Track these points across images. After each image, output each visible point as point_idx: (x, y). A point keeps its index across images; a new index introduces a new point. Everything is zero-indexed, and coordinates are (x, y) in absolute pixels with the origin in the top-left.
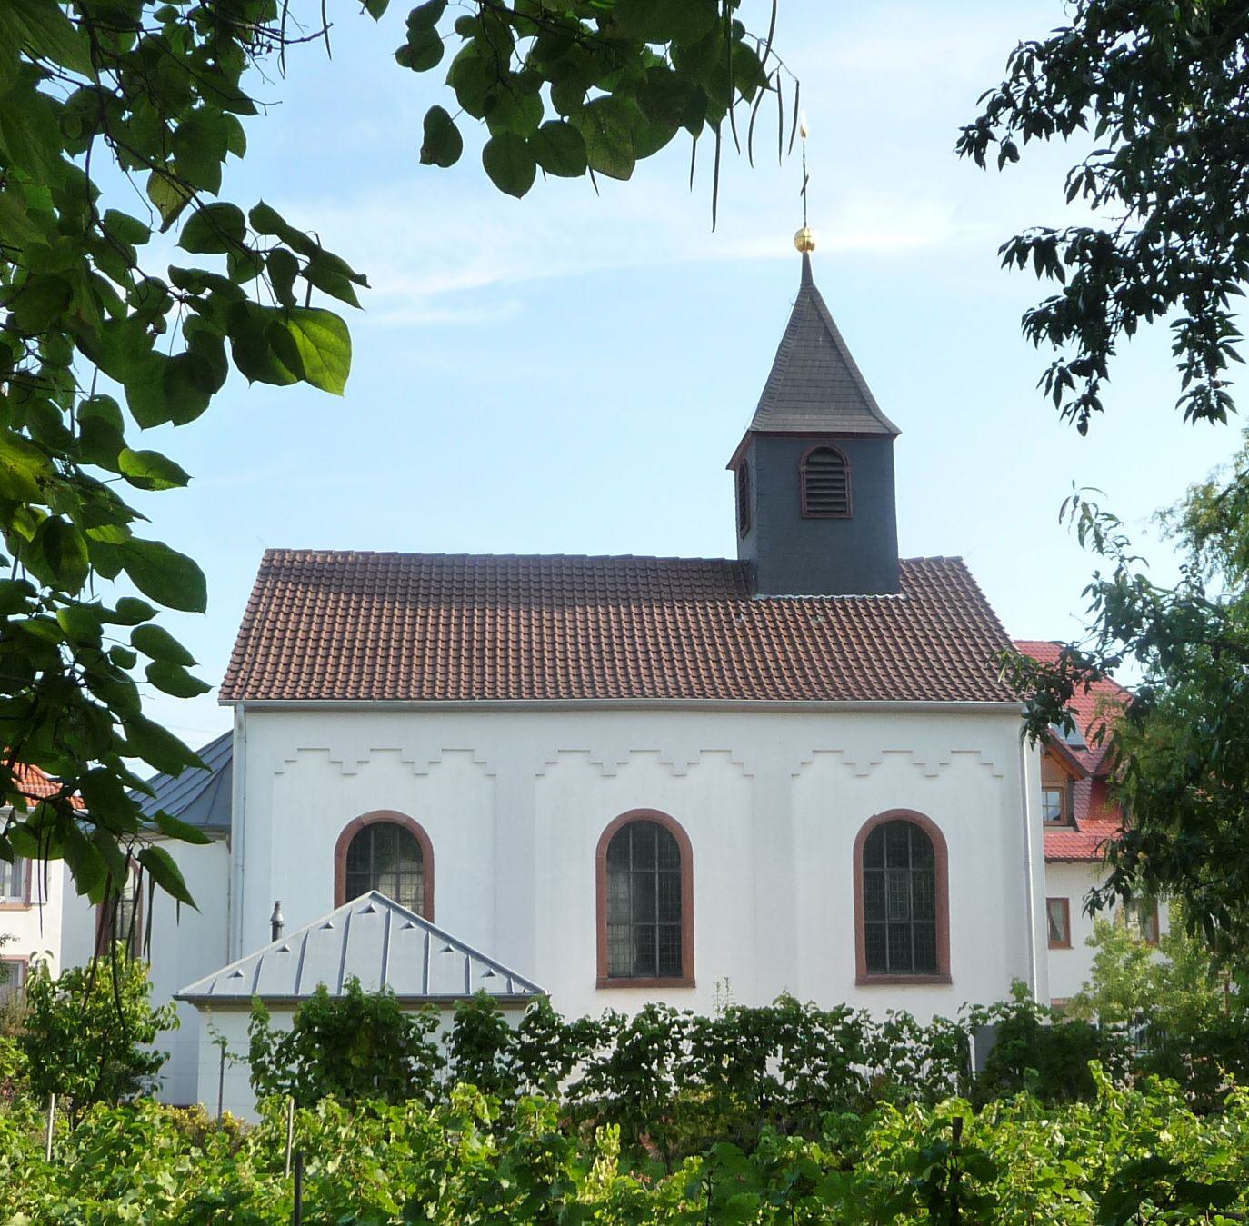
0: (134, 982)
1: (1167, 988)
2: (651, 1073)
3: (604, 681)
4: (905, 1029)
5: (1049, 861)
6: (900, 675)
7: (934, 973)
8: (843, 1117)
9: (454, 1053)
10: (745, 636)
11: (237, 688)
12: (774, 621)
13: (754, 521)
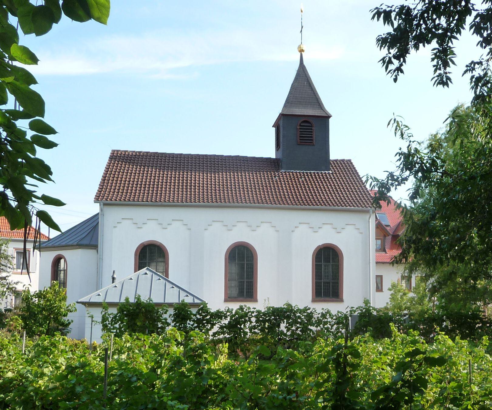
0: (60, 296)
1: (414, 305)
2: (241, 328)
3: (229, 198)
4: (328, 315)
5: (377, 263)
6: (329, 198)
7: (338, 298)
8: (306, 343)
9: (173, 321)
10: (277, 184)
11: (100, 197)
12: (287, 179)
13: (281, 145)
